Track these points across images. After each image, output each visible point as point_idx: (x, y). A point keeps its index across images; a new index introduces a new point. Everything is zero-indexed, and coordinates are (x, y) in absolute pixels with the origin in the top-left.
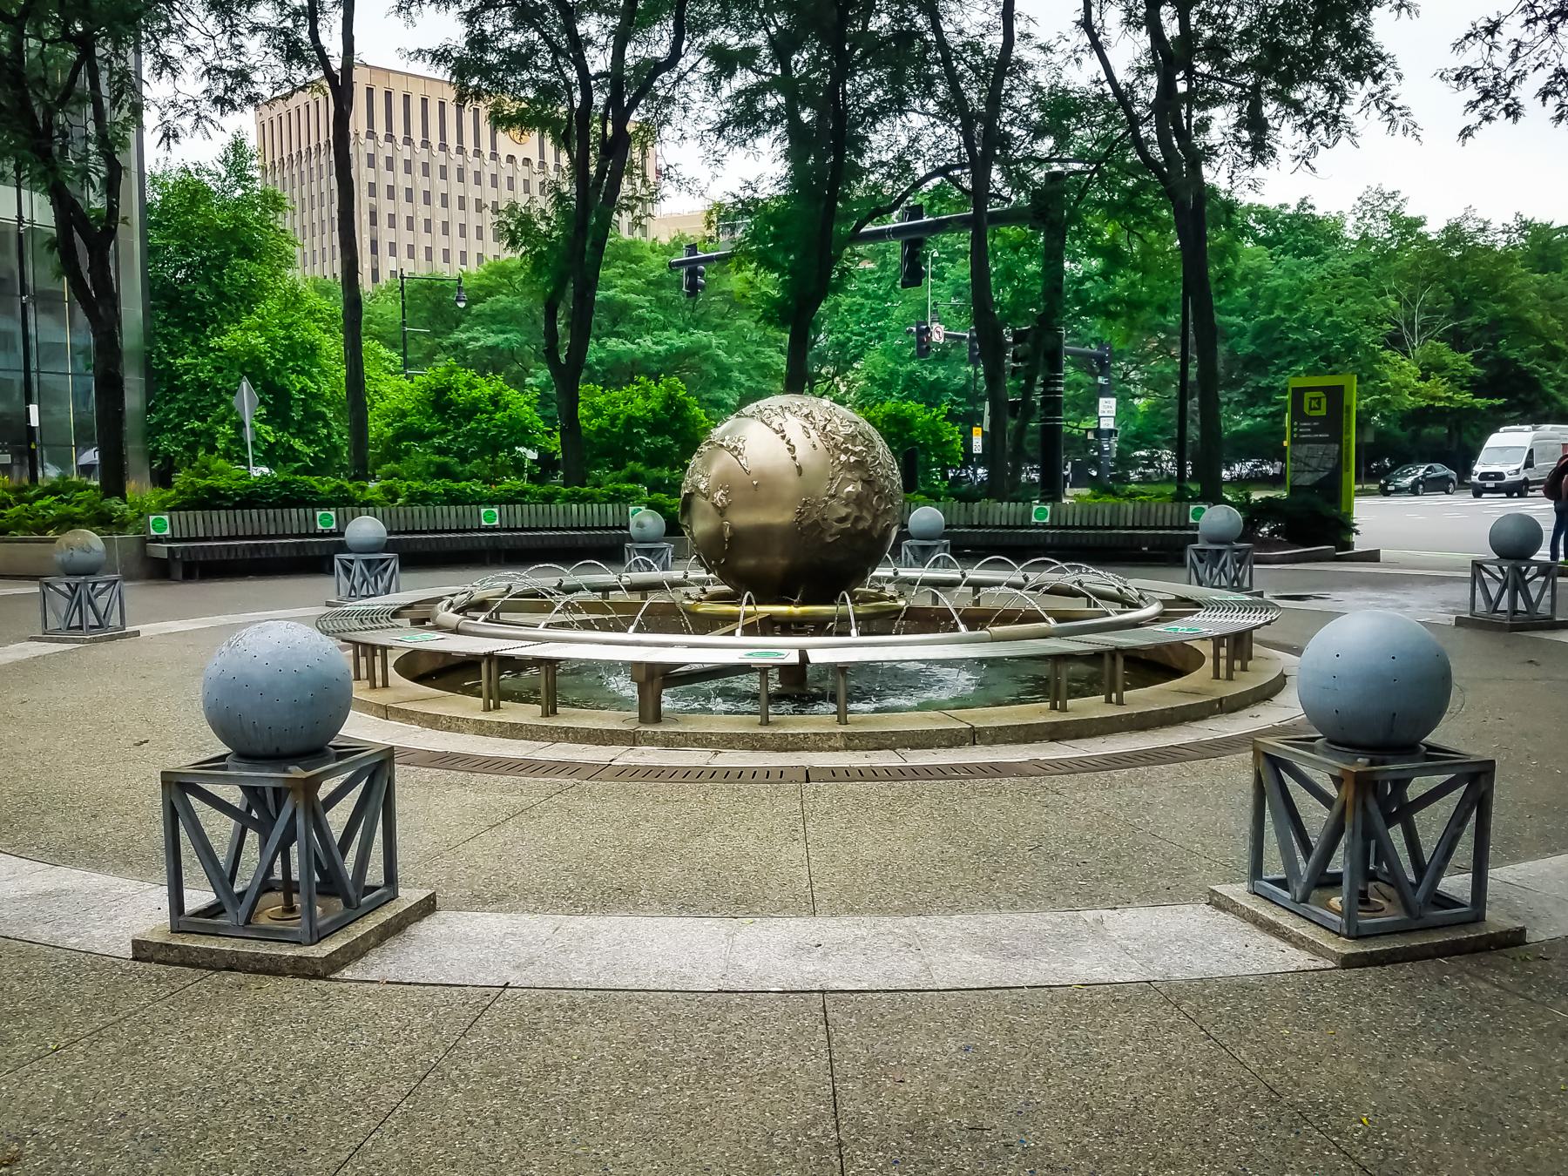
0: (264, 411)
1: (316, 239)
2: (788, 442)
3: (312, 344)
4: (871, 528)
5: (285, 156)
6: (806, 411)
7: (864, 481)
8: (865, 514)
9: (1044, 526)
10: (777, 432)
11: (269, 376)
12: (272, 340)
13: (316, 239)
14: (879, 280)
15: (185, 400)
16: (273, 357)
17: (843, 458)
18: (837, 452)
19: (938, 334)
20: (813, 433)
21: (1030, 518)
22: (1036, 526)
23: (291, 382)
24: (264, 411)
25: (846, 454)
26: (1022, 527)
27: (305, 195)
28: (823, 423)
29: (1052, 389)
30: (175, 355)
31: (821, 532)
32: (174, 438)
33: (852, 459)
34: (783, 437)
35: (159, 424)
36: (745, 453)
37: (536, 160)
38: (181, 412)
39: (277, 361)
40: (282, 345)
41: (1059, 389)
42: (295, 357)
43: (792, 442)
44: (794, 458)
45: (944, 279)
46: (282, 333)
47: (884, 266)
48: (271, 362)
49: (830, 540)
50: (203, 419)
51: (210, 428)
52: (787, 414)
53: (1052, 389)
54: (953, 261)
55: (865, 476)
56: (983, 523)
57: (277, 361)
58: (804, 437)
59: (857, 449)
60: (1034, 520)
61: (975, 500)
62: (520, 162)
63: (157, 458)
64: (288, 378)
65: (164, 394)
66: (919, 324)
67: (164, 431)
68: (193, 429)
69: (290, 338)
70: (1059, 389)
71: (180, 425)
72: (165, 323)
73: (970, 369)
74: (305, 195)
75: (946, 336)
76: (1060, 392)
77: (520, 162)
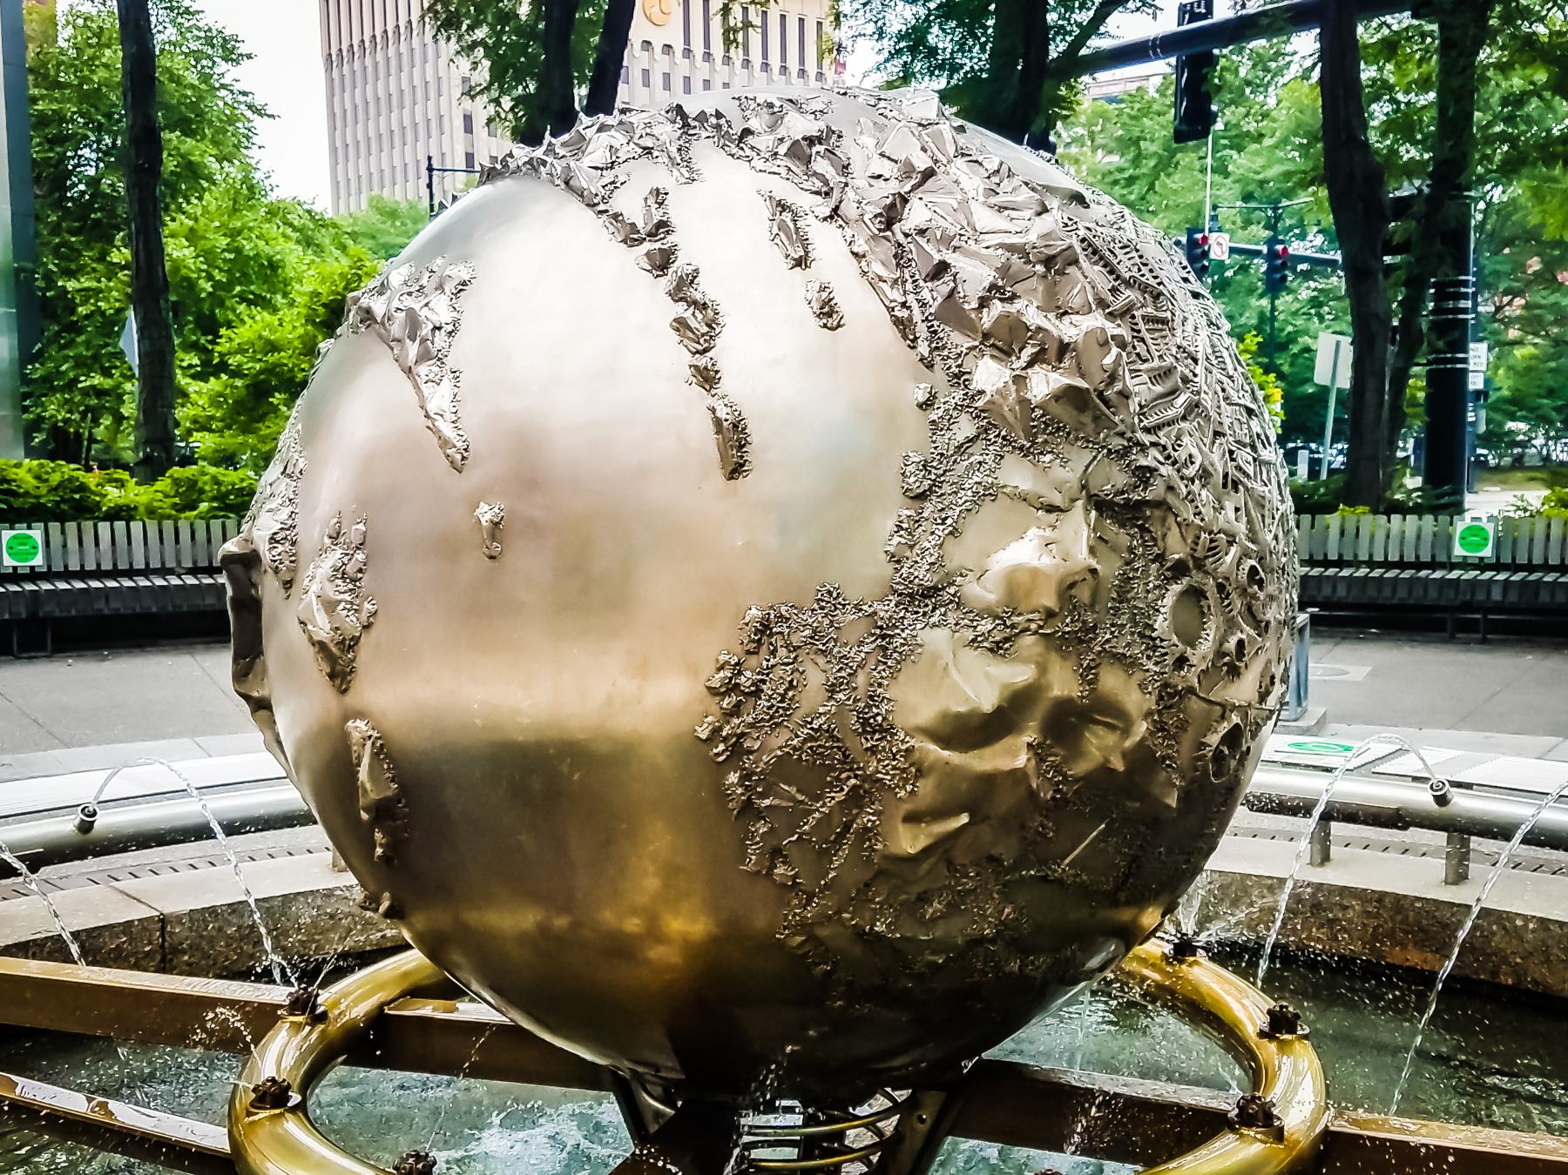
0: (196, 361)
1: (396, 152)
2: (682, 290)
3: (270, 260)
4: (1143, 760)
5: (345, 48)
6: (798, 126)
7: (1101, 505)
8: (1112, 681)
9: (1482, 565)
10: (631, 237)
11: (206, 307)
12: (209, 255)
13: (396, 152)
14: (1131, 181)
15: (87, 344)
16: (210, 277)
17: (989, 375)
18: (959, 340)
19: (1219, 248)
20: (827, 242)
21: (1449, 549)
22: (1465, 565)
23: (238, 316)
24: (196, 361)
25: (1005, 353)
26: (1433, 565)
27: (381, 93)
28: (883, 192)
29: (1451, 304)
30: (70, 274)
31: (856, 799)
32: (67, 401)
33: (1044, 383)
34: (662, 262)
35: (47, 379)
36: (461, 352)
37: (679, 47)
38: (79, 363)
39: (217, 285)
40: (225, 260)
41: (1463, 304)
42: (245, 279)
43: (706, 288)
44: (707, 378)
45: (1227, 175)
46: (224, 242)
47: (1136, 161)
48: (208, 287)
49: (909, 841)
50: (106, 373)
51: (118, 386)
52: (705, 151)
53: (1451, 304)
54: (1240, 149)
55: (1114, 479)
56: (1348, 557)
57: (217, 285)
58: (774, 258)
59: (1069, 330)
60: (1459, 551)
61: (1330, 509)
62: (658, 48)
63: (39, 430)
64: (234, 310)
65: (58, 335)
66: (1191, 232)
67: (54, 390)
68: (93, 387)
69: (238, 251)
70: (1463, 304)
71: (76, 381)
72: (56, 230)
73: (1265, 302)
74: (381, 93)
75: (1232, 251)
76: (1465, 311)
77: (658, 48)
